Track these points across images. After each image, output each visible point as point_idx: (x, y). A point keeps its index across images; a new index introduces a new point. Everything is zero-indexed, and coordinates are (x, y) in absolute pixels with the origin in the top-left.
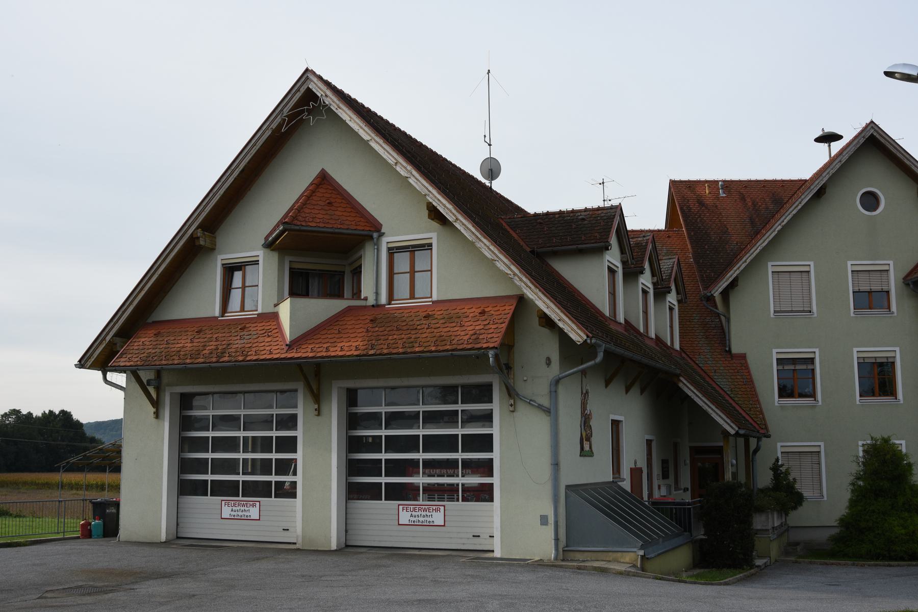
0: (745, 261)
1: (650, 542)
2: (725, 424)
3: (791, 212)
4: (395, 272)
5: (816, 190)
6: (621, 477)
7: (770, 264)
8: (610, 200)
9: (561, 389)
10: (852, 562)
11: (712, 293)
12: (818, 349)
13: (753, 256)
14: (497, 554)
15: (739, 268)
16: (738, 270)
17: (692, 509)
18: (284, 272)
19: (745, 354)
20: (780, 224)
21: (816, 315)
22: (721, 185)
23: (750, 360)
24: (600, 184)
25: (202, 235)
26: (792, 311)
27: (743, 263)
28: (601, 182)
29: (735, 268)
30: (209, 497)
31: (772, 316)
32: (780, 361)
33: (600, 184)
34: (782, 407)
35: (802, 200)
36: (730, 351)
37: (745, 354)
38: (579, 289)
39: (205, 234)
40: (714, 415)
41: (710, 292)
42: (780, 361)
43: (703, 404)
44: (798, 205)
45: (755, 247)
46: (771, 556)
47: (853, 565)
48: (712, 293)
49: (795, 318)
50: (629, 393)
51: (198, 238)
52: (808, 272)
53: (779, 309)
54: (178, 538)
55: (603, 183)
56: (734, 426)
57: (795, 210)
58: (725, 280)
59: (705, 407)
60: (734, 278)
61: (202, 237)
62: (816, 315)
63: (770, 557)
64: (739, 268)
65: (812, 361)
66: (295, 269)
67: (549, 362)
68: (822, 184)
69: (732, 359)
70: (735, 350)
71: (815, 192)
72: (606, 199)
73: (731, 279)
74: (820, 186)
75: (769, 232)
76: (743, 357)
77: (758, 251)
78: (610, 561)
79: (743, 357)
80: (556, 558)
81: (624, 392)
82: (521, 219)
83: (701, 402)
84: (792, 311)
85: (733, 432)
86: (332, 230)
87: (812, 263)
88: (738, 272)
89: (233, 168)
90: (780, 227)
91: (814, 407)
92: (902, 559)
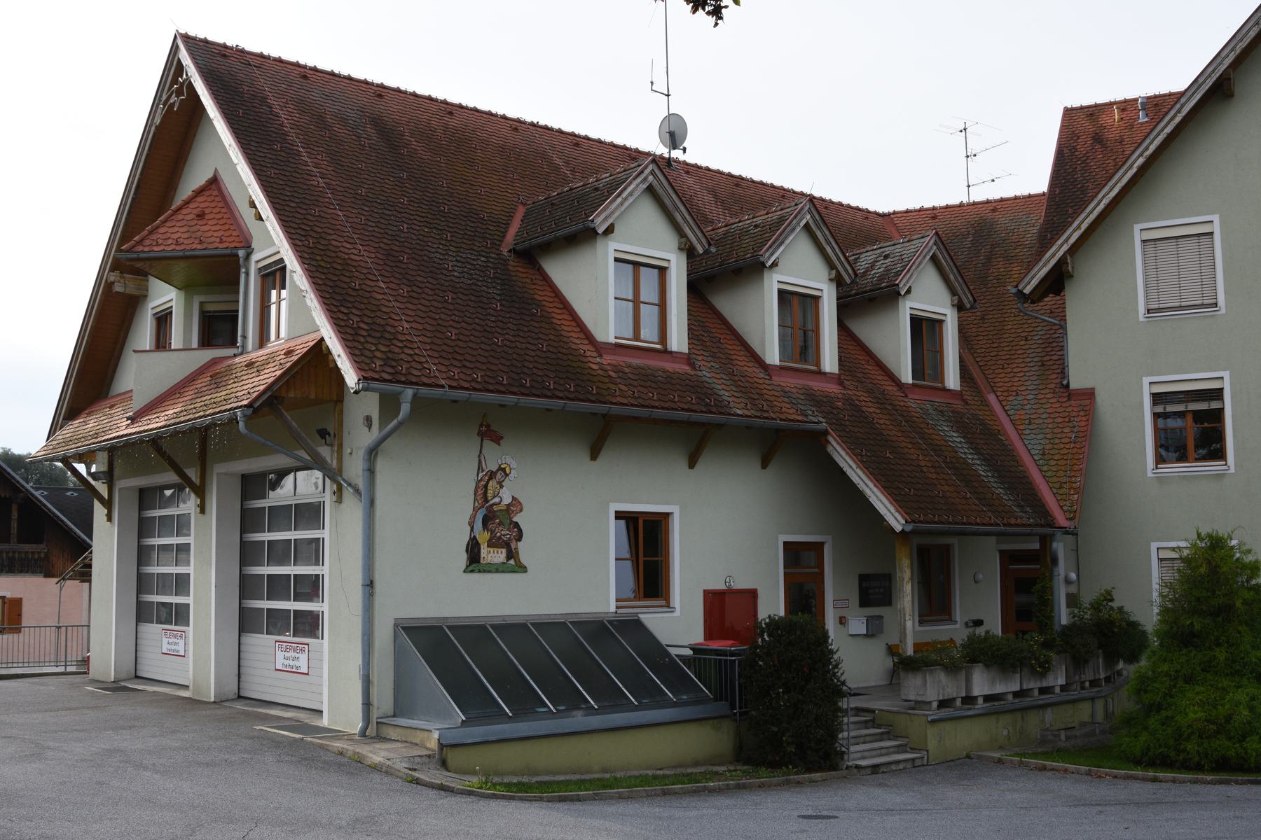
0: (1079, 227)
1: (554, 713)
2: (888, 514)
3: (1162, 130)
4: (657, 307)
5: (1210, 84)
6: (671, 606)
7: (1137, 227)
8: (975, 155)
9: (381, 465)
10: (1087, 768)
11: (1020, 287)
12: (1228, 372)
13: (1093, 217)
14: (325, 722)
15: (1066, 240)
16: (1065, 245)
17: (737, 662)
18: (192, 320)
19: (1094, 389)
20: (1141, 155)
21: (1223, 311)
22: (1141, 103)
23: (1102, 399)
24: (961, 131)
25: (118, 278)
26: (1181, 308)
27: (1074, 231)
28: (962, 129)
29: (1060, 242)
30: (265, 636)
31: (1141, 319)
32: (1157, 398)
33: (961, 131)
34: (1160, 480)
35: (1182, 106)
36: (1068, 386)
37: (1093, 389)
38: (570, 302)
39: (124, 278)
40: (873, 500)
41: (1017, 286)
42: (1157, 398)
43: (860, 481)
44: (1175, 116)
45: (1095, 202)
46: (929, 748)
47: (1089, 773)
48: (1020, 287)
49: (1189, 318)
50: (698, 467)
51: (113, 283)
52: (1212, 233)
53: (1156, 306)
54: (240, 697)
55: (965, 129)
56: (899, 518)
57: (1169, 126)
58: (1041, 264)
59: (862, 486)
60: (1060, 259)
61: (119, 282)
62: (1223, 311)
63: (927, 751)
64: (1066, 240)
65: (1217, 394)
66: (210, 312)
67: (368, 420)
68: (1221, 72)
69: (1069, 400)
70: (1077, 381)
71: (1207, 87)
72: (969, 154)
73: (1053, 262)
74: (1218, 75)
75: (1121, 171)
76: (1089, 394)
77: (1102, 206)
78: (416, 744)
79: (1089, 394)
80: (363, 733)
81: (758, 465)
82: (546, 201)
83: (857, 478)
84: (1181, 308)
85: (898, 528)
86: (229, 251)
87: (1216, 218)
88: (1065, 248)
89: (129, 185)
90: (1141, 161)
91: (1220, 477)
92: (1199, 768)
